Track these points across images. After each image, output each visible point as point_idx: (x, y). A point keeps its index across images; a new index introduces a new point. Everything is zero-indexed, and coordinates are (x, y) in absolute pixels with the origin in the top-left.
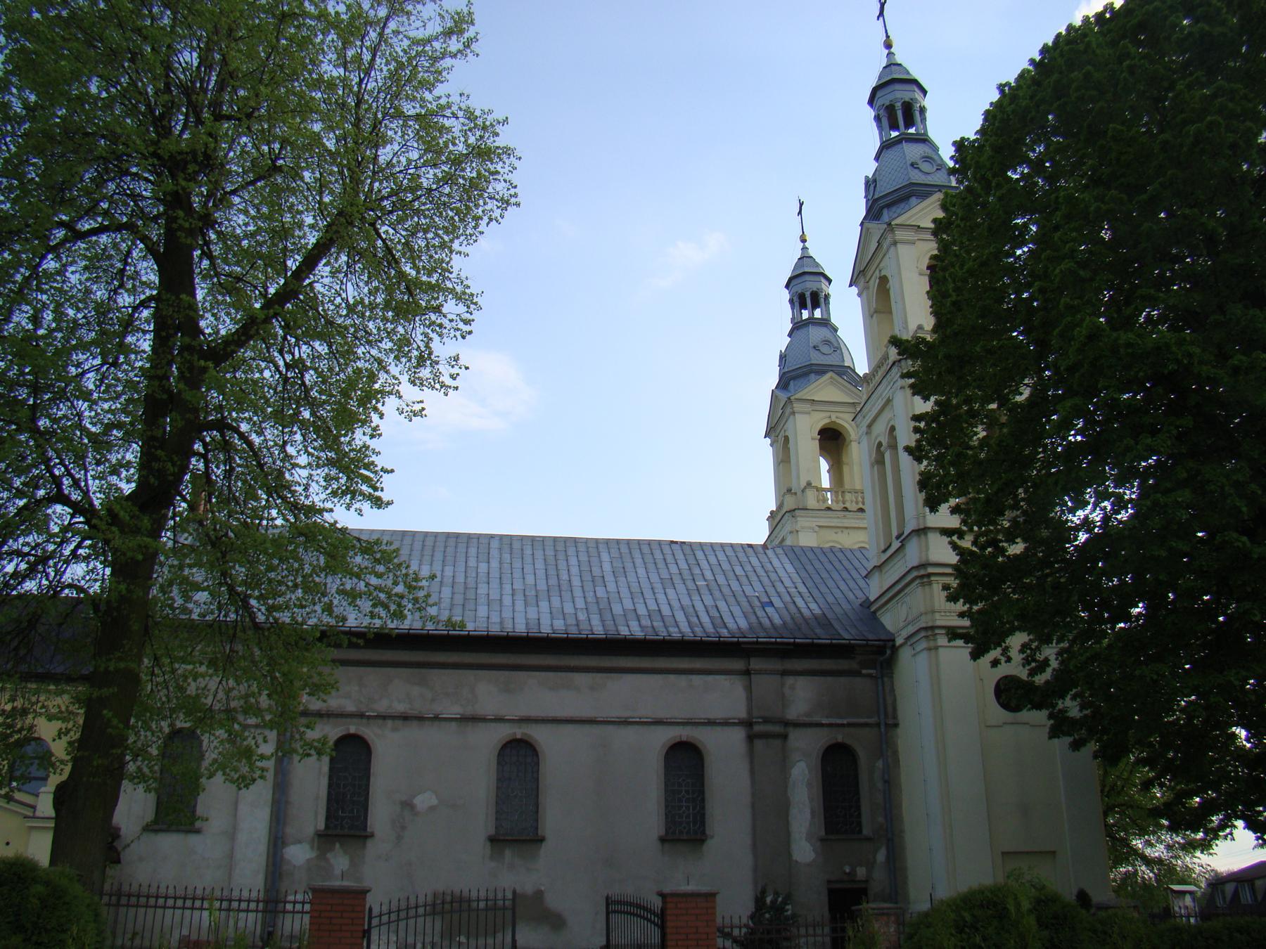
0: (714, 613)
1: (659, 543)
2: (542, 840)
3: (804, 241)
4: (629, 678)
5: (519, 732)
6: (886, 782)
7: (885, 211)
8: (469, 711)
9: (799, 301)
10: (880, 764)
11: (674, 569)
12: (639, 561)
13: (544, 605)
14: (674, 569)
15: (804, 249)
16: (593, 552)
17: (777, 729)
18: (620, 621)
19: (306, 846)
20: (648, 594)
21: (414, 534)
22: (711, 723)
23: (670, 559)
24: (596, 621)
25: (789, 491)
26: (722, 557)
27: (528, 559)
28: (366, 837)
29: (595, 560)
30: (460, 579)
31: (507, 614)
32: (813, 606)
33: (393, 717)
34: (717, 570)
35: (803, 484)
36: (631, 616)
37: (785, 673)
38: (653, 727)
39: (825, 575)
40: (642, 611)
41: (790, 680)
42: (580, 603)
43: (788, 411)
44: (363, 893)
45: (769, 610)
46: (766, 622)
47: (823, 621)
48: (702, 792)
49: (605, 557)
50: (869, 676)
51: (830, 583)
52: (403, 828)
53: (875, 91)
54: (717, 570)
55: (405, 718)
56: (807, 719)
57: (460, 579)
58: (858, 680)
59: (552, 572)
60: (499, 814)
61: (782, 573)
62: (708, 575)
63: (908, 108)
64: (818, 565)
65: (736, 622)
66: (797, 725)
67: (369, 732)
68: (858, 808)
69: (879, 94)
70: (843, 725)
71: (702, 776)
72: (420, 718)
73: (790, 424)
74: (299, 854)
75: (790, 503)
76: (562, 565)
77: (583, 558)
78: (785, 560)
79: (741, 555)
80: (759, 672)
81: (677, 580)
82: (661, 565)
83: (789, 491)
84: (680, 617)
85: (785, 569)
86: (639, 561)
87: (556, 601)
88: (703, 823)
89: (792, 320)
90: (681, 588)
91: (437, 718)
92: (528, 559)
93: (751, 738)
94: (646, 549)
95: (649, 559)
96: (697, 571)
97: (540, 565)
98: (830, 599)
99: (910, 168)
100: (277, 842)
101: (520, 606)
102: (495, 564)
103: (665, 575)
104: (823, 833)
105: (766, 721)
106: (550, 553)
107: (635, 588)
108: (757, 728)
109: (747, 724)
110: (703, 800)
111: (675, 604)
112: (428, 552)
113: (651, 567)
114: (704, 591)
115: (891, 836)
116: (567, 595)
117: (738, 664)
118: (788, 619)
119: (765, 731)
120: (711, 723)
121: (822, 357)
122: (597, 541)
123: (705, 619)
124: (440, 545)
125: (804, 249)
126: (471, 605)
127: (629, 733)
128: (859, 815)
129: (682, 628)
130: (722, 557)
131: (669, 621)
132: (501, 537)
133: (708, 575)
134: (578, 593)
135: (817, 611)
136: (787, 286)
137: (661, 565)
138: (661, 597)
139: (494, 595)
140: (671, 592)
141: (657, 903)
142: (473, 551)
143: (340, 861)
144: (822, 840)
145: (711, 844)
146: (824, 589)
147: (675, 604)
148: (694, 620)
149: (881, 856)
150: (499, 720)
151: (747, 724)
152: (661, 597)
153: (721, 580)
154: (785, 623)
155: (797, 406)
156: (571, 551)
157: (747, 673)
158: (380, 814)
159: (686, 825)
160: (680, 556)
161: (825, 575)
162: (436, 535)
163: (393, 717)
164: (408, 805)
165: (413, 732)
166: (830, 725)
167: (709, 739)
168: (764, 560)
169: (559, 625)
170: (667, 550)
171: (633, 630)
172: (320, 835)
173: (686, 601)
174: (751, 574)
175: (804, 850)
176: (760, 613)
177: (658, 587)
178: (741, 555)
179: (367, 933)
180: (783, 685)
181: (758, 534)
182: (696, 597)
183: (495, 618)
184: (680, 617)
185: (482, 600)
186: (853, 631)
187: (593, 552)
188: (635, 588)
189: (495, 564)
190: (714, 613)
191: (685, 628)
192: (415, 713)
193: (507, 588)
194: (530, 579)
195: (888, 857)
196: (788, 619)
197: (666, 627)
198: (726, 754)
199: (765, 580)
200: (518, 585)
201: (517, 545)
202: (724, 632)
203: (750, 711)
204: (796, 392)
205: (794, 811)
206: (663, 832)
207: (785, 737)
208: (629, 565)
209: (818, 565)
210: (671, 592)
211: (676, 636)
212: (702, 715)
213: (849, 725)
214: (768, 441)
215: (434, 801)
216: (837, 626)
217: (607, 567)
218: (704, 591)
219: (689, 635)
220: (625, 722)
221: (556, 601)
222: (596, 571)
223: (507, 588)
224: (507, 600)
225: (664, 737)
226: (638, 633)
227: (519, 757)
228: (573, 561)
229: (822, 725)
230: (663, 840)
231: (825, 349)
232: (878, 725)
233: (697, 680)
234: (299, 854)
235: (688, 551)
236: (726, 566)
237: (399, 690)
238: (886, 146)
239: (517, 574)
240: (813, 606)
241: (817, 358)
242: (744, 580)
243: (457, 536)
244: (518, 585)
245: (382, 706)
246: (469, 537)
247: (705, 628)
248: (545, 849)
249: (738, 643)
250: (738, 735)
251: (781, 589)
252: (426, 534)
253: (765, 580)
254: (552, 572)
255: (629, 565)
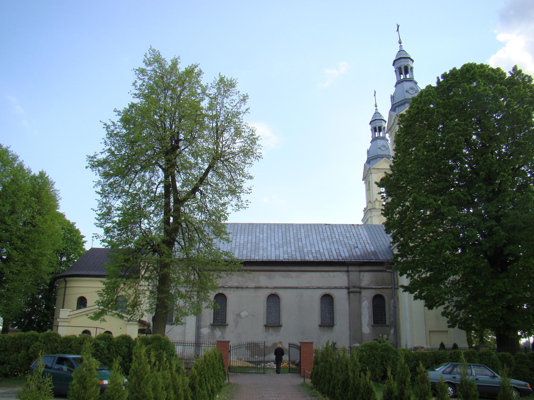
0: (338, 251)
1: (321, 225)
2: (281, 326)
3: (376, 106)
4: (309, 273)
5: (273, 291)
6: (395, 307)
7: (397, 108)
8: (257, 285)
9: (374, 130)
10: (392, 301)
11: (325, 235)
12: (314, 232)
13: (281, 249)
14: (325, 235)
15: (376, 109)
16: (298, 229)
17: (358, 290)
18: (306, 254)
19: (207, 328)
20: (316, 245)
21: (238, 224)
22: (336, 288)
23: (324, 230)
24: (298, 255)
25: (370, 202)
26: (342, 230)
27: (276, 232)
28: (226, 325)
29: (299, 232)
30: (254, 241)
31: (269, 253)
32: (372, 248)
33: (233, 288)
34: (340, 234)
35: (375, 199)
36: (310, 253)
37: (360, 271)
38: (317, 290)
39: (378, 236)
40: (314, 251)
41: (362, 273)
42: (293, 249)
43: (369, 172)
44: (228, 342)
45: (357, 249)
46: (355, 254)
47: (374, 253)
48: (333, 310)
49: (302, 231)
50: (389, 272)
51: (379, 239)
52: (237, 322)
53: (395, 61)
54: (340, 234)
55: (237, 288)
56: (367, 286)
57: (254, 241)
58: (385, 273)
59: (284, 237)
60: (268, 318)
61: (363, 235)
62: (337, 237)
63: (406, 68)
64: (376, 232)
65: (345, 254)
66: (365, 288)
67: (226, 292)
68: (385, 315)
69: (396, 63)
70: (380, 288)
71: (333, 305)
72: (242, 288)
73: (370, 177)
74: (205, 331)
75: (370, 206)
76: (288, 234)
77: (295, 231)
78: (365, 230)
79: (349, 229)
80: (352, 271)
81: (326, 239)
82: (321, 233)
83: (370, 202)
84: (326, 253)
85: (364, 234)
86: (314, 232)
87: (285, 248)
88: (333, 320)
89: (372, 137)
90: (327, 242)
91: (247, 288)
92: (276, 232)
93: (349, 293)
94: (316, 228)
95: (317, 231)
96: (333, 235)
97: (280, 235)
98: (378, 245)
99: (406, 93)
100: (198, 327)
101: (273, 250)
102: (265, 235)
103: (322, 237)
104: (373, 324)
105: (354, 287)
106: (284, 230)
107: (312, 243)
108: (351, 290)
109: (348, 288)
110: (333, 313)
111: (325, 248)
112: (243, 231)
113: (318, 234)
114: (335, 243)
115: (396, 325)
116: (289, 246)
117: (345, 269)
118: (362, 253)
119: (353, 290)
120: (336, 288)
121: (382, 152)
122: (300, 224)
123: (334, 253)
124: (247, 228)
125: (376, 109)
126: (257, 250)
127: (309, 291)
128: (385, 318)
129: (326, 257)
130: (342, 230)
131: (322, 254)
132: (267, 224)
133: (337, 237)
134: (293, 245)
135: (373, 250)
136: (370, 124)
137: (321, 233)
138: (320, 245)
139: (265, 246)
140: (324, 243)
141: (299, 344)
142: (258, 230)
143: (218, 333)
144: (372, 326)
145: (335, 327)
146: (376, 241)
147: (325, 248)
148: (331, 253)
149: (392, 331)
150: (267, 288)
151: (348, 288)
152: (320, 245)
153: (341, 238)
154: (361, 254)
155: (373, 171)
156: (291, 229)
157: (348, 271)
158: (230, 318)
159: (328, 322)
160: (328, 230)
161: (378, 236)
162: (245, 224)
163: (233, 288)
164: (239, 315)
165: (240, 292)
166: (375, 288)
167: (334, 293)
168: (357, 230)
169: (286, 257)
170: (324, 227)
171: (310, 258)
172: (212, 325)
173: (329, 247)
174: (352, 236)
175: (366, 329)
176: (353, 251)
177: (320, 241)
178: (349, 229)
179: (230, 351)
180: (360, 275)
181: (357, 219)
182: (332, 245)
183: (265, 255)
184: (326, 253)
185: (261, 248)
186: (384, 257)
187: (298, 229)
188: (312, 243)
189: (265, 235)
190: (338, 251)
191: (328, 257)
192: (240, 286)
193: (269, 243)
194: (277, 240)
195: (394, 333)
196: (362, 253)
197: (321, 256)
198: (341, 299)
199: (357, 238)
200: (273, 242)
201: (272, 227)
202: (340, 258)
203: (349, 284)
204: (373, 165)
205: (363, 317)
206: (320, 323)
207: (360, 292)
208: (310, 234)
209: (376, 232)
210: (324, 243)
211: (324, 260)
212: (333, 285)
213: (382, 288)
214: (364, 182)
215: (247, 314)
216: (379, 255)
217: (303, 235)
218: (335, 243)
219: (328, 260)
220: (308, 288)
221: (285, 248)
222: (299, 236)
223: (269, 243)
224: (269, 248)
225: (320, 293)
226: (312, 259)
227: (273, 299)
228: (292, 233)
229: (373, 288)
230: (320, 326)
231: (383, 149)
232: (392, 288)
233: (331, 274)
234: (205, 331)
235: (331, 228)
236: (344, 233)
237: (235, 279)
238: (399, 83)
239: (273, 238)
240: (372, 248)
241: (380, 153)
242: (349, 238)
243: (253, 224)
244: (273, 242)
245: (230, 284)
246: (256, 224)
247: (334, 257)
248: (282, 328)
249: (345, 262)
250: (345, 291)
251: (362, 241)
252: (242, 224)
253: (357, 238)
254: (284, 237)
255: (310, 234)
